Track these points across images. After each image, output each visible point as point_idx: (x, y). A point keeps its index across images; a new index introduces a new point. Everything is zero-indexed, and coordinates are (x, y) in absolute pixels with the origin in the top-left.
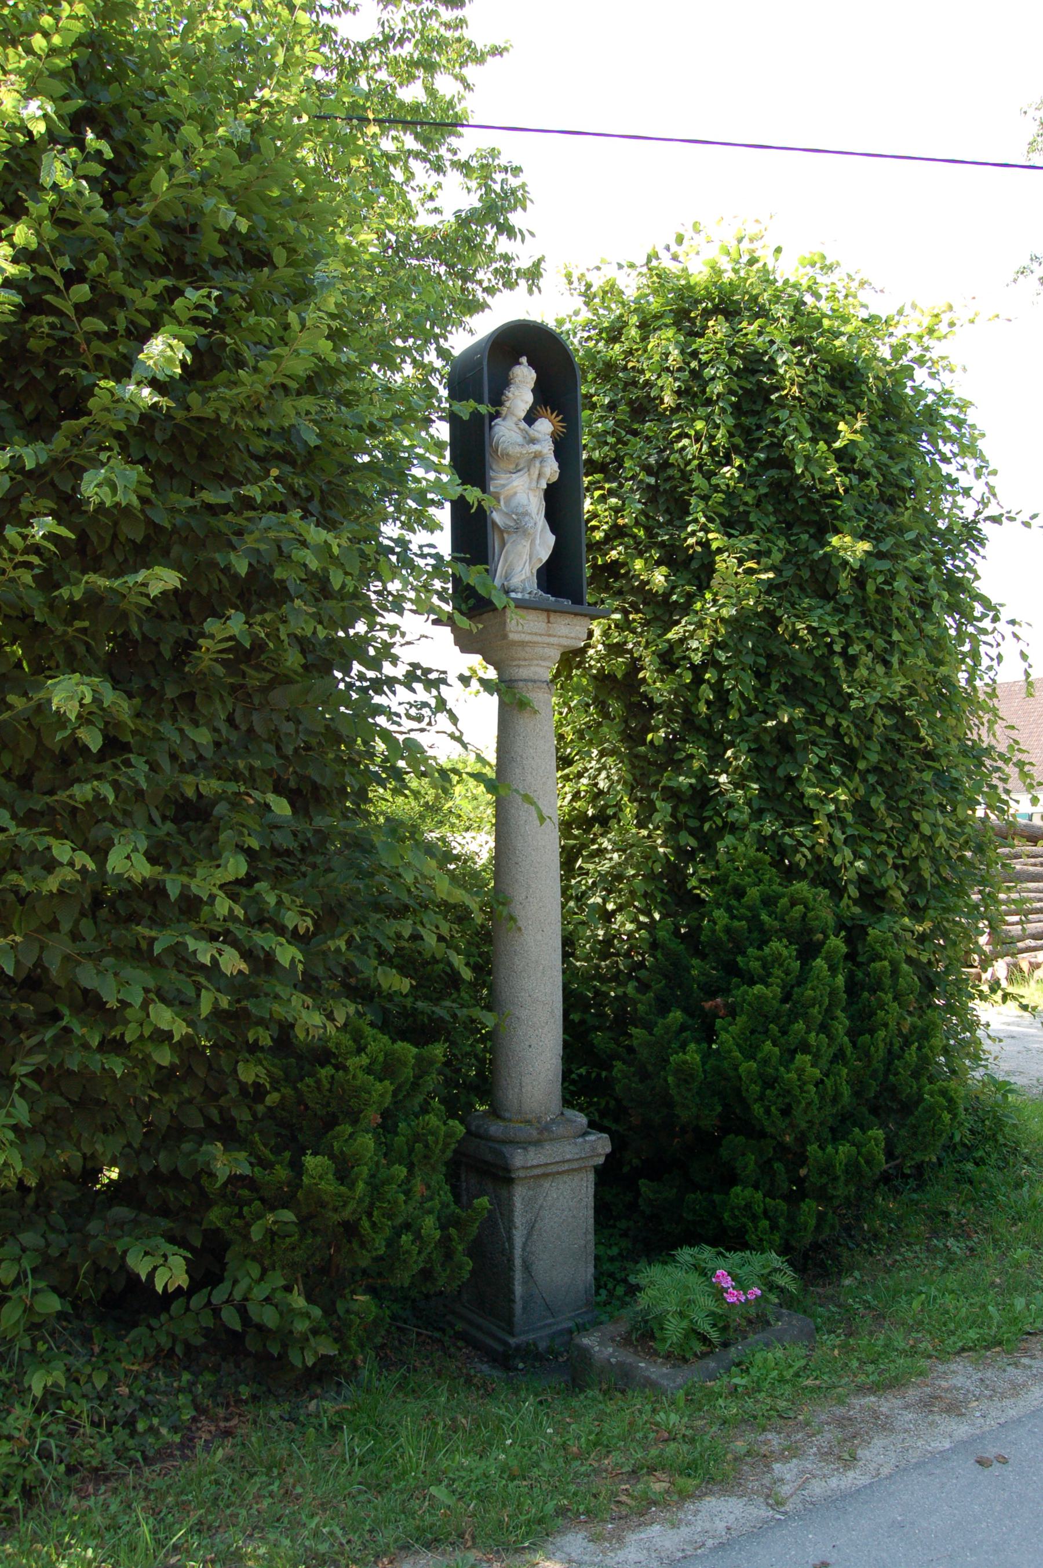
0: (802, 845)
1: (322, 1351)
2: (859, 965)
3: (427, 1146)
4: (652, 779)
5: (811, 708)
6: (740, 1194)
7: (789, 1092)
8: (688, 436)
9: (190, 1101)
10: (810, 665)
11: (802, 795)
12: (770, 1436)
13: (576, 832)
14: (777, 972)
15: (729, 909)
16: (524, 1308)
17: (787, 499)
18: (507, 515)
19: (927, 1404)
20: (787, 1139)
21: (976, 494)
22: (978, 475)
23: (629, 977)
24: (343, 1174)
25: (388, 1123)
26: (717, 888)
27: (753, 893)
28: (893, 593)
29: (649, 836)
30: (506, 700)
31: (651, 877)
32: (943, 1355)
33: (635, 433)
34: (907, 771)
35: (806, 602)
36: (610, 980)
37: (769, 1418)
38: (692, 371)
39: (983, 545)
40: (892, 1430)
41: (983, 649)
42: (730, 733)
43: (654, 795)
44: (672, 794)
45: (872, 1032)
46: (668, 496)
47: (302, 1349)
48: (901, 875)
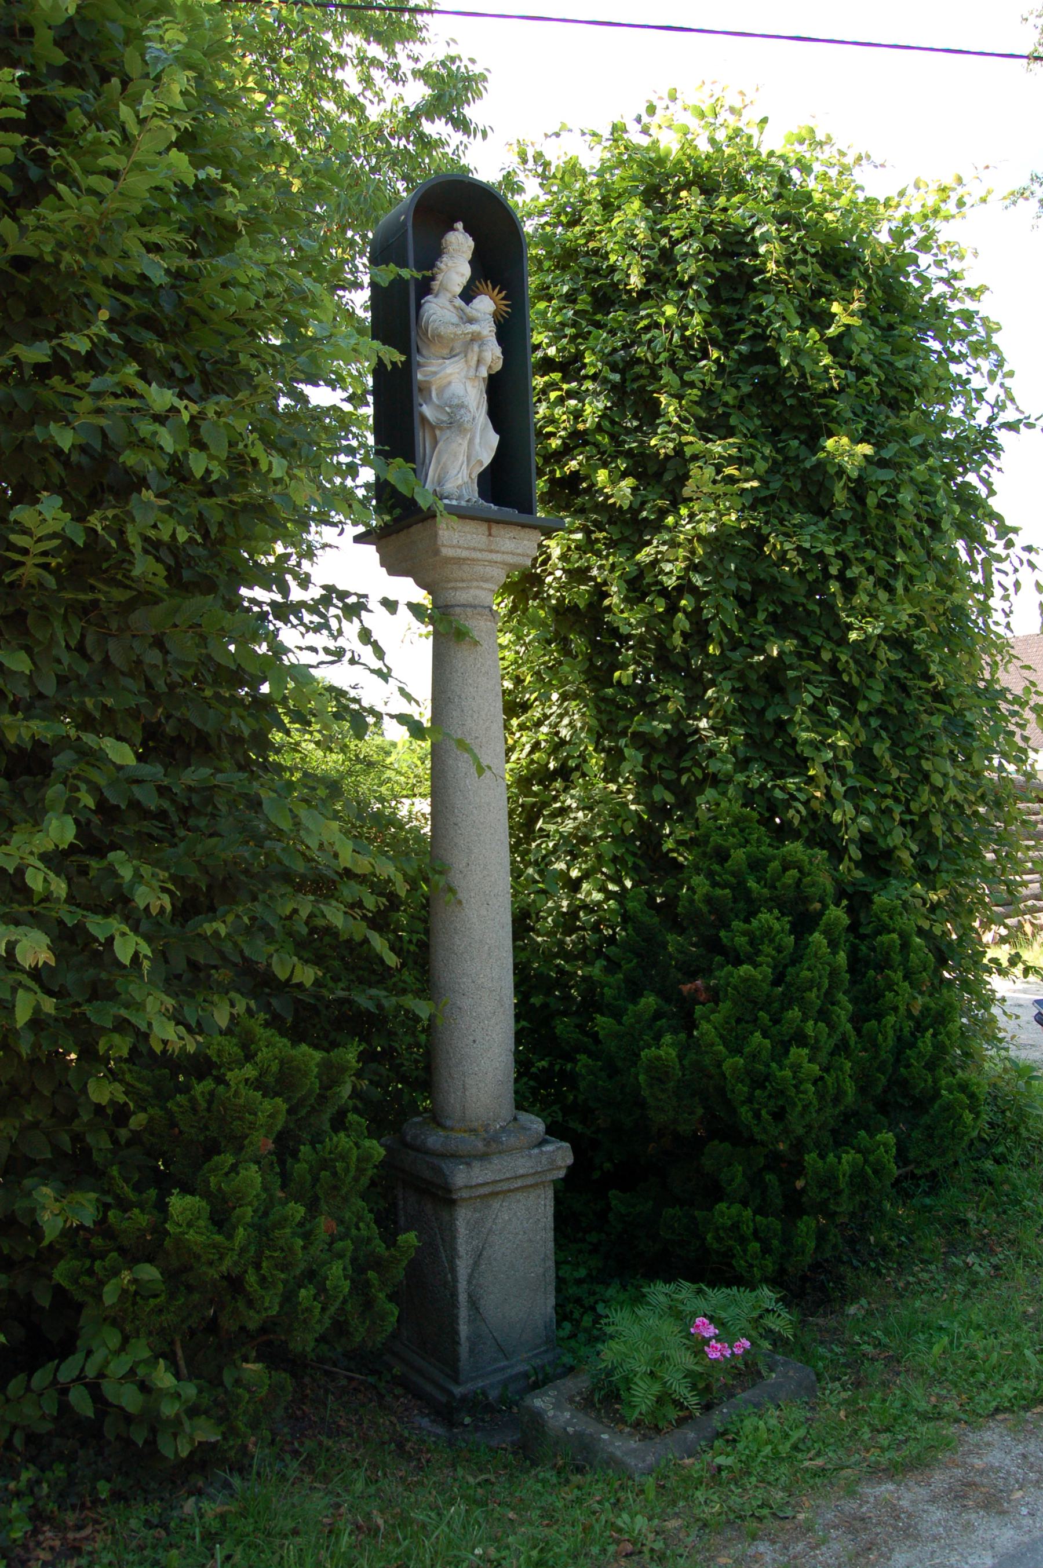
0: (797, 799)
1: (200, 1437)
2: (863, 937)
3: (335, 1174)
4: (621, 725)
5: (804, 641)
6: (725, 1212)
7: (782, 1092)
8: (657, 325)
9: (36, 1125)
10: (803, 591)
11: (795, 741)
12: (762, 1547)
13: (535, 788)
14: (767, 949)
15: (710, 874)
16: (471, 1351)
17: (774, 401)
18: (440, 408)
19: (959, 1495)
20: (781, 1147)
21: (990, 396)
22: (992, 376)
23: (599, 953)
24: (221, 1219)
25: (285, 1145)
26: (697, 851)
27: (739, 855)
28: (897, 506)
29: (619, 791)
30: (441, 629)
31: (621, 838)
32: (973, 1418)
33: (598, 325)
34: (915, 715)
35: (797, 518)
36: (576, 958)
37: (760, 1519)
38: (663, 250)
39: (997, 456)
40: (917, 1537)
41: (996, 577)
42: (710, 671)
43: (622, 742)
44: (641, 741)
45: (879, 1017)
46: (633, 392)
47: (175, 1435)
48: (909, 833)
